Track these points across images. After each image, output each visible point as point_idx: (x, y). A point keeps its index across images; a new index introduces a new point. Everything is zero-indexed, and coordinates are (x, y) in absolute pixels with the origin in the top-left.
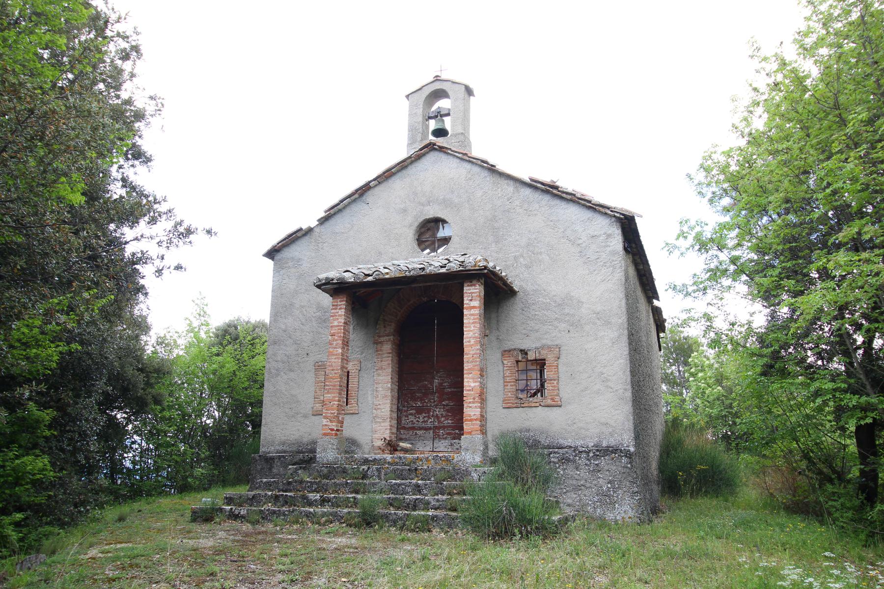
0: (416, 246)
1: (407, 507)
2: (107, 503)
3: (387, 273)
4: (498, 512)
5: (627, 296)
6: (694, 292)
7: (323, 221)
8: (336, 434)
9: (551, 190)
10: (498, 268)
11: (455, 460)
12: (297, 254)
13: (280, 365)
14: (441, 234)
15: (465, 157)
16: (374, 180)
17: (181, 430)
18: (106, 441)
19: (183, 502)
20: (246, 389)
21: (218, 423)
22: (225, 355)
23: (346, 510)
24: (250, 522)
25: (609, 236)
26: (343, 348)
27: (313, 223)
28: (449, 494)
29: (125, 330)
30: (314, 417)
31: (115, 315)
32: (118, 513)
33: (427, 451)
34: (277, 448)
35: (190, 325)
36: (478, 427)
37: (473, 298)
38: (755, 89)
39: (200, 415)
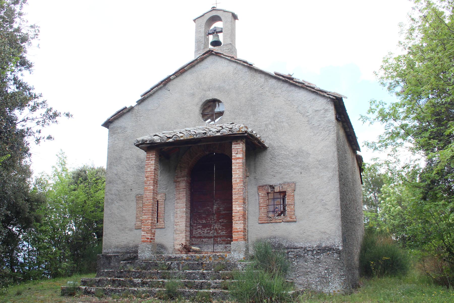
0: (201, 118)
1: (196, 287)
2: (9, 283)
3: (182, 137)
4: (254, 290)
5: (338, 150)
6: (380, 147)
7: (140, 102)
8: (150, 242)
9: (288, 81)
10: (254, 132)
11: (227, 258)
12: (124, 124)
13: (114, 197)
14: (217, 110)
15: (232, 59)
16: (173, 75)
17: (52, 238)
18: (8, 245)
19: (56, 284)
20: (93, 212)
21: (76, 234)
23: (157, 289)
24: (98, 297)
25: (326, 110)
26: (154, 186)
27: (134, 104)
28: (223, 279)
29: (16, 174)
30: (136, 231)
31: (11, 166)
32: (17, 290)
33: (209, 252)
34: (113, 250)
35: (56, 171)
36: (242, 236)
37: (238, 152)
38: (413, 19)
39: (65, 229)
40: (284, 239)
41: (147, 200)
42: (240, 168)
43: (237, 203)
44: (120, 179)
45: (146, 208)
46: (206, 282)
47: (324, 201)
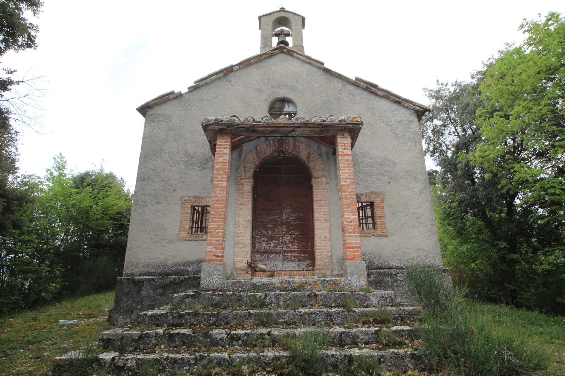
7: (193, 89)
9: (370, 88)
16: (237, 65)
22: (83, 194)
27: (184, 90)
34: (142, 270)
40: (375, 256)
41: (218, 201)
42: (350, 167)
43: (349, 209)
44: (158, 176)
45: (216, 211)
46: (349, 333)
47: (417, 215)
